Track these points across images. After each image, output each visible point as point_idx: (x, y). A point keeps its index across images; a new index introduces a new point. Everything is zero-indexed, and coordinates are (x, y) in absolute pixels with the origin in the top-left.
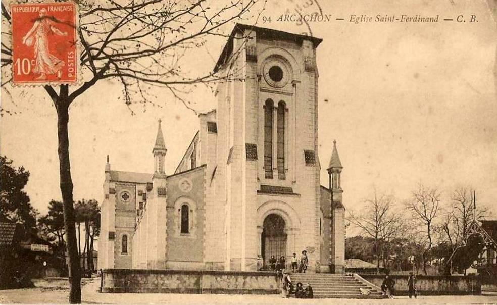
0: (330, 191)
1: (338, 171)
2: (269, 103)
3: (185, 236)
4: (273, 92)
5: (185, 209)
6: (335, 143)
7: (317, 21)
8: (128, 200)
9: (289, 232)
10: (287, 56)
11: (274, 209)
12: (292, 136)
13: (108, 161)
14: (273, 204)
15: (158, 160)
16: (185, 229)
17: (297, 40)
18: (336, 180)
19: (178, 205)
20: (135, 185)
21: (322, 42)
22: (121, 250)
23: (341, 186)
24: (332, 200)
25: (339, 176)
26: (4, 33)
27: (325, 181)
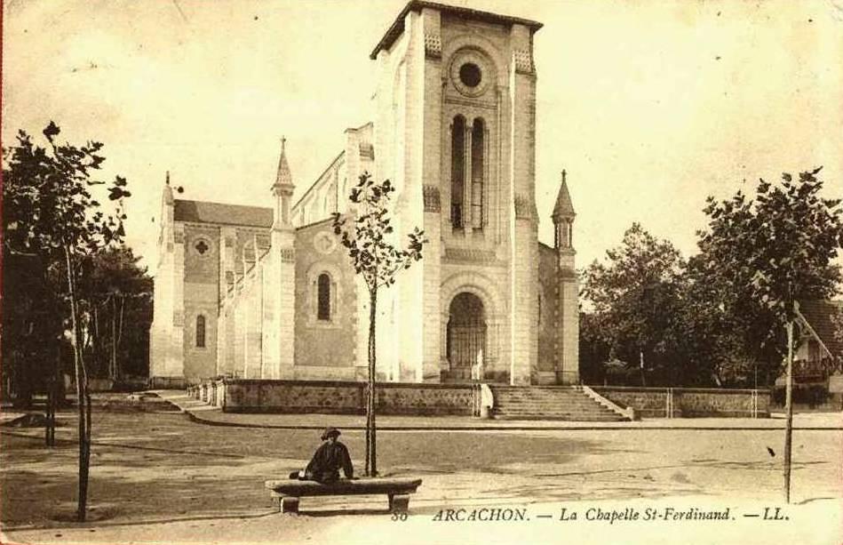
0: (556, 251)
1: (568, 220)
2: (459, 122)
3: (325, 325)
4: (465, 104)
5: (324, 282)
6: (564, 174)
7: (513, 510)
8: (206, 252)
9: (489, 322)
10: (488, 48)
11: (472, 286)
12: (496, 147)
13: (168, 182)
14: (465, 277)
15: (281, 201)
16: (324, 313)
17: (505, 24)
18: (566, 235)
19: (313, 277)
20: (219, 228)
21: (542, 29)
22: (194, 342)
23: (573, 246)
24: (558, 266)
25: (571, 226)
26: (717, 515)
27: (547, 235)
